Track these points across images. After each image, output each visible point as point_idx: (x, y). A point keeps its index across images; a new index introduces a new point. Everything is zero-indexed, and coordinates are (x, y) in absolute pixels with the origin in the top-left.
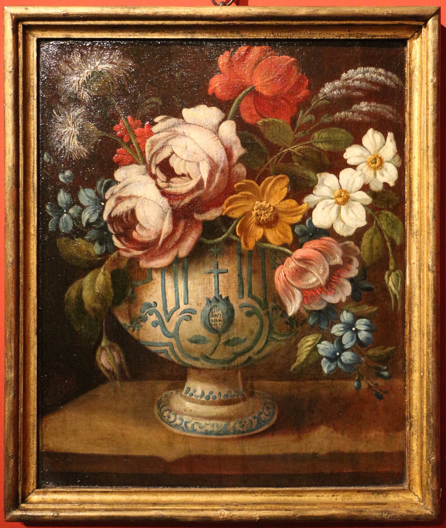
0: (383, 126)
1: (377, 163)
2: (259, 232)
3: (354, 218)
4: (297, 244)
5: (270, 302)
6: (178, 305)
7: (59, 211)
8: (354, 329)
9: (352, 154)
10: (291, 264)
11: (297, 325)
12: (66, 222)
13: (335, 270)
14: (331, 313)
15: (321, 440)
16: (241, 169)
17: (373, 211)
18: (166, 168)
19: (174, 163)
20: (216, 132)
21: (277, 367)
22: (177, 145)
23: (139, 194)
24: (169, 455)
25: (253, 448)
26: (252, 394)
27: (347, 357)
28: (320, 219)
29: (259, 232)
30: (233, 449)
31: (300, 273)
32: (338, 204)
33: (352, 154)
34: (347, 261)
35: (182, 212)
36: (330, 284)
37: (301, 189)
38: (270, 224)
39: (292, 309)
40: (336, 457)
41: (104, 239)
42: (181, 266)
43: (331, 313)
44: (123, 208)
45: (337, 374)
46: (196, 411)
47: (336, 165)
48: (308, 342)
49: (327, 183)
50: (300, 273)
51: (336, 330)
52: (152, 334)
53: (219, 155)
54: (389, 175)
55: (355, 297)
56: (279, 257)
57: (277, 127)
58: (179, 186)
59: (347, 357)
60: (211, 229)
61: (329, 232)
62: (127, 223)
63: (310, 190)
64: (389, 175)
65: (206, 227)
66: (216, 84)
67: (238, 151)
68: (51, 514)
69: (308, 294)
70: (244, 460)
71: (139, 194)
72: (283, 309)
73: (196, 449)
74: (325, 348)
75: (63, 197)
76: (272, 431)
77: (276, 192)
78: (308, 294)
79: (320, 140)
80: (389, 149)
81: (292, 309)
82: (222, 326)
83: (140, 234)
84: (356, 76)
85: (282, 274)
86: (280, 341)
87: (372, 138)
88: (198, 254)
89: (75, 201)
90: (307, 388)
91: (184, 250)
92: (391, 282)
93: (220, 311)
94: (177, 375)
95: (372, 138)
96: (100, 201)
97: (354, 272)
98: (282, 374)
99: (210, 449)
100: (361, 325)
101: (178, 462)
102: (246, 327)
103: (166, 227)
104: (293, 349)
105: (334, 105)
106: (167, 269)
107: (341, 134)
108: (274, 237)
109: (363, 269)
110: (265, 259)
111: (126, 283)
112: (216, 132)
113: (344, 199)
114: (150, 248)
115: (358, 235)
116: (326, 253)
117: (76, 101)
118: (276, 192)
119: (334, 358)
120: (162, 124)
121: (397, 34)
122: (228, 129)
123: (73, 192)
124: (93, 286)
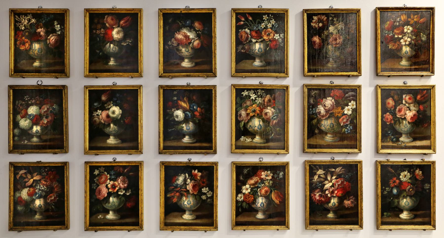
0: (354, 100)
1: (353, 105)
2: (337, 114)
3: (350, 112)
4: (342, 116)
5: (339, 124)
6: (326, 124)
7: (310, 111)
8: (350, 128)
9: (350, 104)
10: (341, 119)
11: (342, 127)
12: (311, 113)
13: (347, 120)
14: (347, 125)
15: (345, 143)
16: (335, 106)
17: (352, 112)
18: (325, 105)
19: (326, 105)
20: (331, 100)
21: (340, 133)
22: (326, 103)
23: (321, 109)
24: (325, 144)
25: (336, 143)
26: (326, 112)
27: (349, 131)
28: (345, 112)
29: (337, 114)
30: (334, 144)
31: (343, 120)
32: (348, 111)
33: (350, 104)
34: (349, 118)
35: (327, 111)
36: (347, 121)
37: (343, 108)
38: (338, 113)
39: (342, 125)
40: (348, 145)
41: (316, 115)
42: (327, 119)
43: (347, 125)
44: (319, 111)
45: (348, 134)
46: (329, 138)
47: (347, 105)
48: (344, 129)
49: (346, 108)
50: (343, 120)
51: (348, 128)
52: (323, 128)
53: (332, 103)
54: (355, 107)
55: (350, 123)
56: (340, 118)
57: (340, 100)
58: (327, 108)
59: (349, 131)
60: (331, 114)
61: (347, 114)
62: (320, 113)
63: (344, 109)
64: (355, 107)
65: (330, 114)
66: (332, 94)
67: (334, 103)
68: (401, 159)
69: (344, 123)
70: (335, 145)
71: (321, 109)
72: (340, 125)
73: (328, 144)
74: (346, 130)
75: (311, 109)
76: (339, 141)
77: (339, 109)
78: (344, 123)
79: (345, 102)
80: (355, 103)
81: (342, 125)
82: (332, 127)
83: (321, 114)
84: (350, 93)
85: (340, 120)
86: (340, 129)
87: (352, 102)
88: (329, 117)
89: (312, 110)
90: (344, 135)
91: (327, 117)
92: (355, 121)
93: (332, 125)
94: (326, 134)
95: (352, 102)
96: (316, 110)
97: (350, 120)
98: (340, 134)
99: (330, 144)
100: (351, 127)
101: (326, 145)
102: (335, 127)
103: (325, 113)
104: (342, 130)
105: (347, 97)
106: (325, 119)
107: (348, 101)
108: (339, 115)
109: (351, 119)
110: (338, 118)
111: (319, 121)
112: (331, 100)
113: (349, 110)
114: (323, 116)
115: (351, 115)
116: (346, 117)
117: (312, 96)
118: (339, 109)
119: (347, 132)
120: (324, 100)
121: (344, 159)
122: (333, 100)
123: (312, 109)
124: (315, 121)
